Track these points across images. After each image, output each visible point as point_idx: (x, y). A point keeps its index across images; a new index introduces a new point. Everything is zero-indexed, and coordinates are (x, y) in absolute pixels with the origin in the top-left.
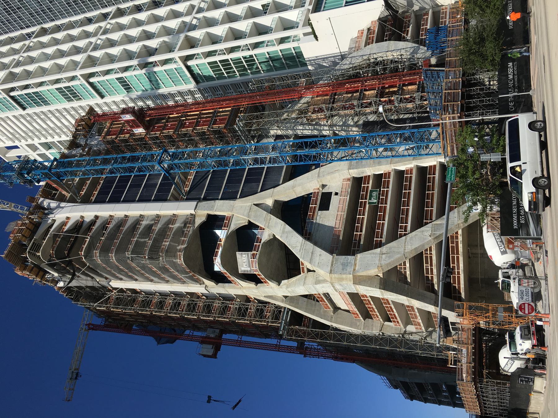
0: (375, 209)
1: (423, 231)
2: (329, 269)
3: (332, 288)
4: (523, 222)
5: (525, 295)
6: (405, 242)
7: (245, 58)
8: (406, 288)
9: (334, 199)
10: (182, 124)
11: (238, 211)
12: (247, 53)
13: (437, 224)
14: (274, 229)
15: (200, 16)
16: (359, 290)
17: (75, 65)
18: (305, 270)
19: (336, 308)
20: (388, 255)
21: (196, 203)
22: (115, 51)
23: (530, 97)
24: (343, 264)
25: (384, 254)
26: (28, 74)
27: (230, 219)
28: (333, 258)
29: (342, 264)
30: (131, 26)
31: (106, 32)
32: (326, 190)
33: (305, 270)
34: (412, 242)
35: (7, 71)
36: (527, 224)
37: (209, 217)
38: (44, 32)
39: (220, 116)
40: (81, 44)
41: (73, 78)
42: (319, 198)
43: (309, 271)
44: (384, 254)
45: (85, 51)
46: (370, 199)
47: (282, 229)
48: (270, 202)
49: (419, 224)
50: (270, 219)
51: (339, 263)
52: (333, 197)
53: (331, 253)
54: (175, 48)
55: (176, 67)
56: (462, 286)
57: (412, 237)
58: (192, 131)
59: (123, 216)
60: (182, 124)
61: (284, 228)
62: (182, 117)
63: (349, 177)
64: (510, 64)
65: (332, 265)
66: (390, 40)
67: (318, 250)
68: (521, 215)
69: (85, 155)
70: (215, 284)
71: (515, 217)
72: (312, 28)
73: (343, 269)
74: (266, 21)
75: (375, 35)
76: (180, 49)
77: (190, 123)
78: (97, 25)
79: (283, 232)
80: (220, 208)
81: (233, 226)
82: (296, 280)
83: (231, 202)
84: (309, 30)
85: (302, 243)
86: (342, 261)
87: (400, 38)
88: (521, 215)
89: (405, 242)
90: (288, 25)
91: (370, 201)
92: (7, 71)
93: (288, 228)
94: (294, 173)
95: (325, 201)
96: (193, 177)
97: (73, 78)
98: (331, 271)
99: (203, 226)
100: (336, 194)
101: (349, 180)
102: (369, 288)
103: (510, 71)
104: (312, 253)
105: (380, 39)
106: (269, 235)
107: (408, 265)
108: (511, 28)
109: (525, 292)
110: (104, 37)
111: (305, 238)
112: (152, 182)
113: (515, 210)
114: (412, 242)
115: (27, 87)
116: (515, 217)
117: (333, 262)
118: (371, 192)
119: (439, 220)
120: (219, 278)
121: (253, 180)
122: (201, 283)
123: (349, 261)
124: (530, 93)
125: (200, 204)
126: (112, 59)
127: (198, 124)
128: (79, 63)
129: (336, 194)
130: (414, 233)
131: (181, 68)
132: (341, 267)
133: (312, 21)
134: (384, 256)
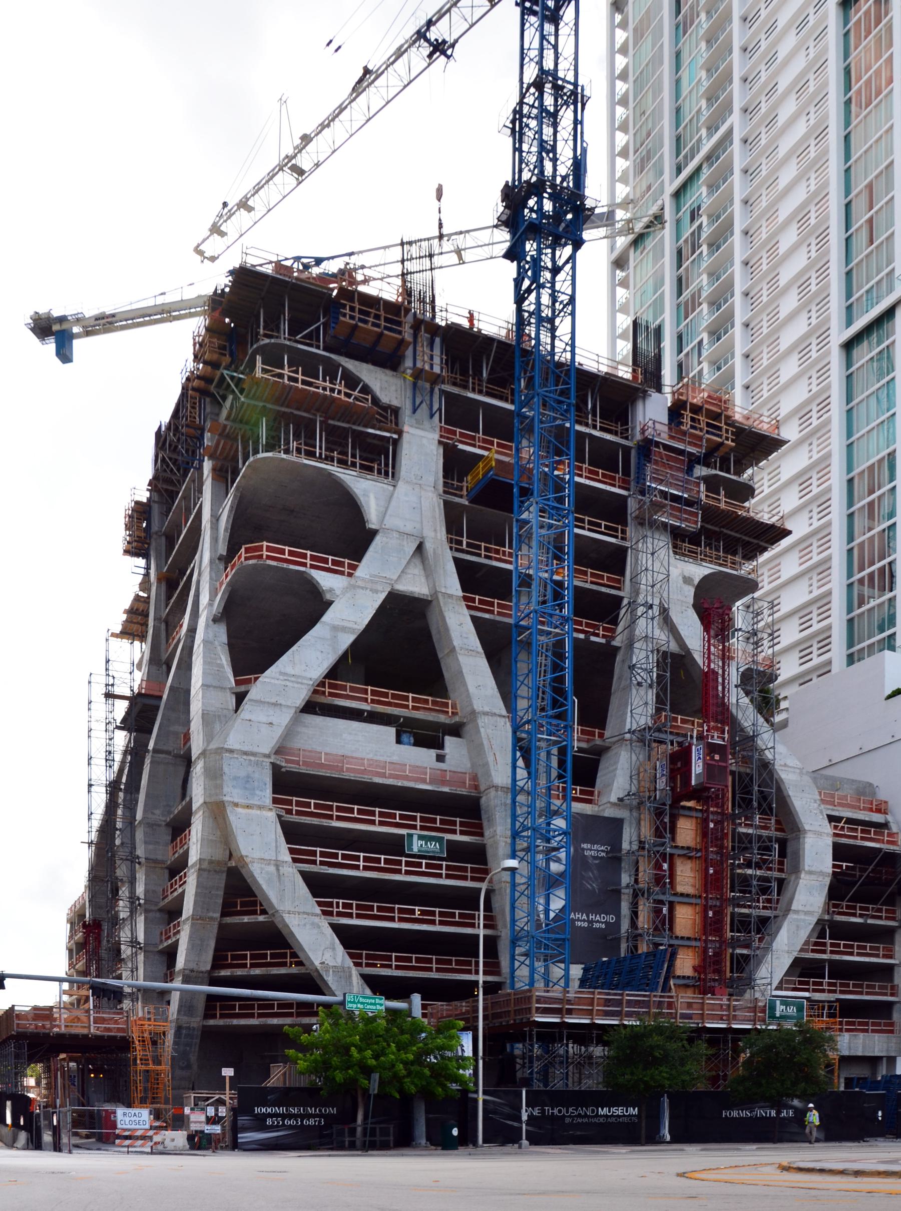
0: (396, 846)
1: (334, 949)
4: (269, 1122)
5: (133, 1119)
6: (308, 914)
8: (211, 914)
13: (350, 976)
14: (351, 604)
16: (197, 816)
18: (242, 688)
20: (275, 879)
24: (248, 779)
25: (278, 870)
28: (265, 756)
29: (248, 777)
33: (242, 688)
34: (308, 926)
36: (264, 1128)
44: (278, 870)
46: (421, 837)
47: (346, 624)
49: (350, 938)
50: (376, 592)
51: (250, 769)
52: (433, 753)
56: (235, 1022)
57: (319, 927)
61: (344, 629)
63: (482, 788)
65: (246, 753)
68: (283, 1121)
71: (282, 1110)
82: (222, 666)
85: (305, 678)
88: (283, 1121)
89: (308, 914)
91: (415, 838)
101: (476, 787)
104: (275, 705)
106: (331, 590)
107: (261, 918)
109: (138, 1119)
114: (308, 926)
117: (254, 754)
118: (440, 840)
119: (361, 981)
123: (258, 792)
124: (525, 1142)
130: (329, 931)
134: (272, 869)
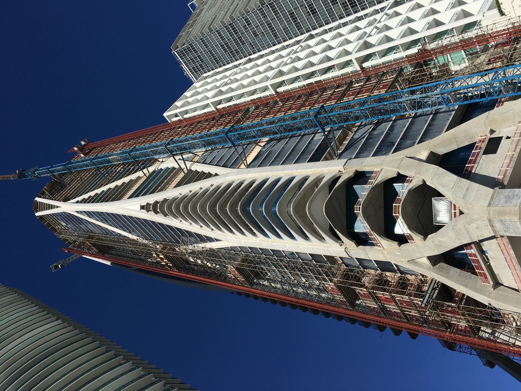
3: (490, 228)
9: (504, 145)
19: (497, 284)
29: (506, 197)
32: (494, 136)
39: (383, 83)
48: (424, 155)
52: (504, 142)
69: (210, 26)
70: (355, 245)
73: (506, 202)
80: (368, 163)
86: (506, 194)
92: (218, 90)
100: (508, 138)
104: (467, 189)
111: (460, 176)
120: (362, 240)
123: (516, 194)
129: (508, 138)
132: (504, 200)
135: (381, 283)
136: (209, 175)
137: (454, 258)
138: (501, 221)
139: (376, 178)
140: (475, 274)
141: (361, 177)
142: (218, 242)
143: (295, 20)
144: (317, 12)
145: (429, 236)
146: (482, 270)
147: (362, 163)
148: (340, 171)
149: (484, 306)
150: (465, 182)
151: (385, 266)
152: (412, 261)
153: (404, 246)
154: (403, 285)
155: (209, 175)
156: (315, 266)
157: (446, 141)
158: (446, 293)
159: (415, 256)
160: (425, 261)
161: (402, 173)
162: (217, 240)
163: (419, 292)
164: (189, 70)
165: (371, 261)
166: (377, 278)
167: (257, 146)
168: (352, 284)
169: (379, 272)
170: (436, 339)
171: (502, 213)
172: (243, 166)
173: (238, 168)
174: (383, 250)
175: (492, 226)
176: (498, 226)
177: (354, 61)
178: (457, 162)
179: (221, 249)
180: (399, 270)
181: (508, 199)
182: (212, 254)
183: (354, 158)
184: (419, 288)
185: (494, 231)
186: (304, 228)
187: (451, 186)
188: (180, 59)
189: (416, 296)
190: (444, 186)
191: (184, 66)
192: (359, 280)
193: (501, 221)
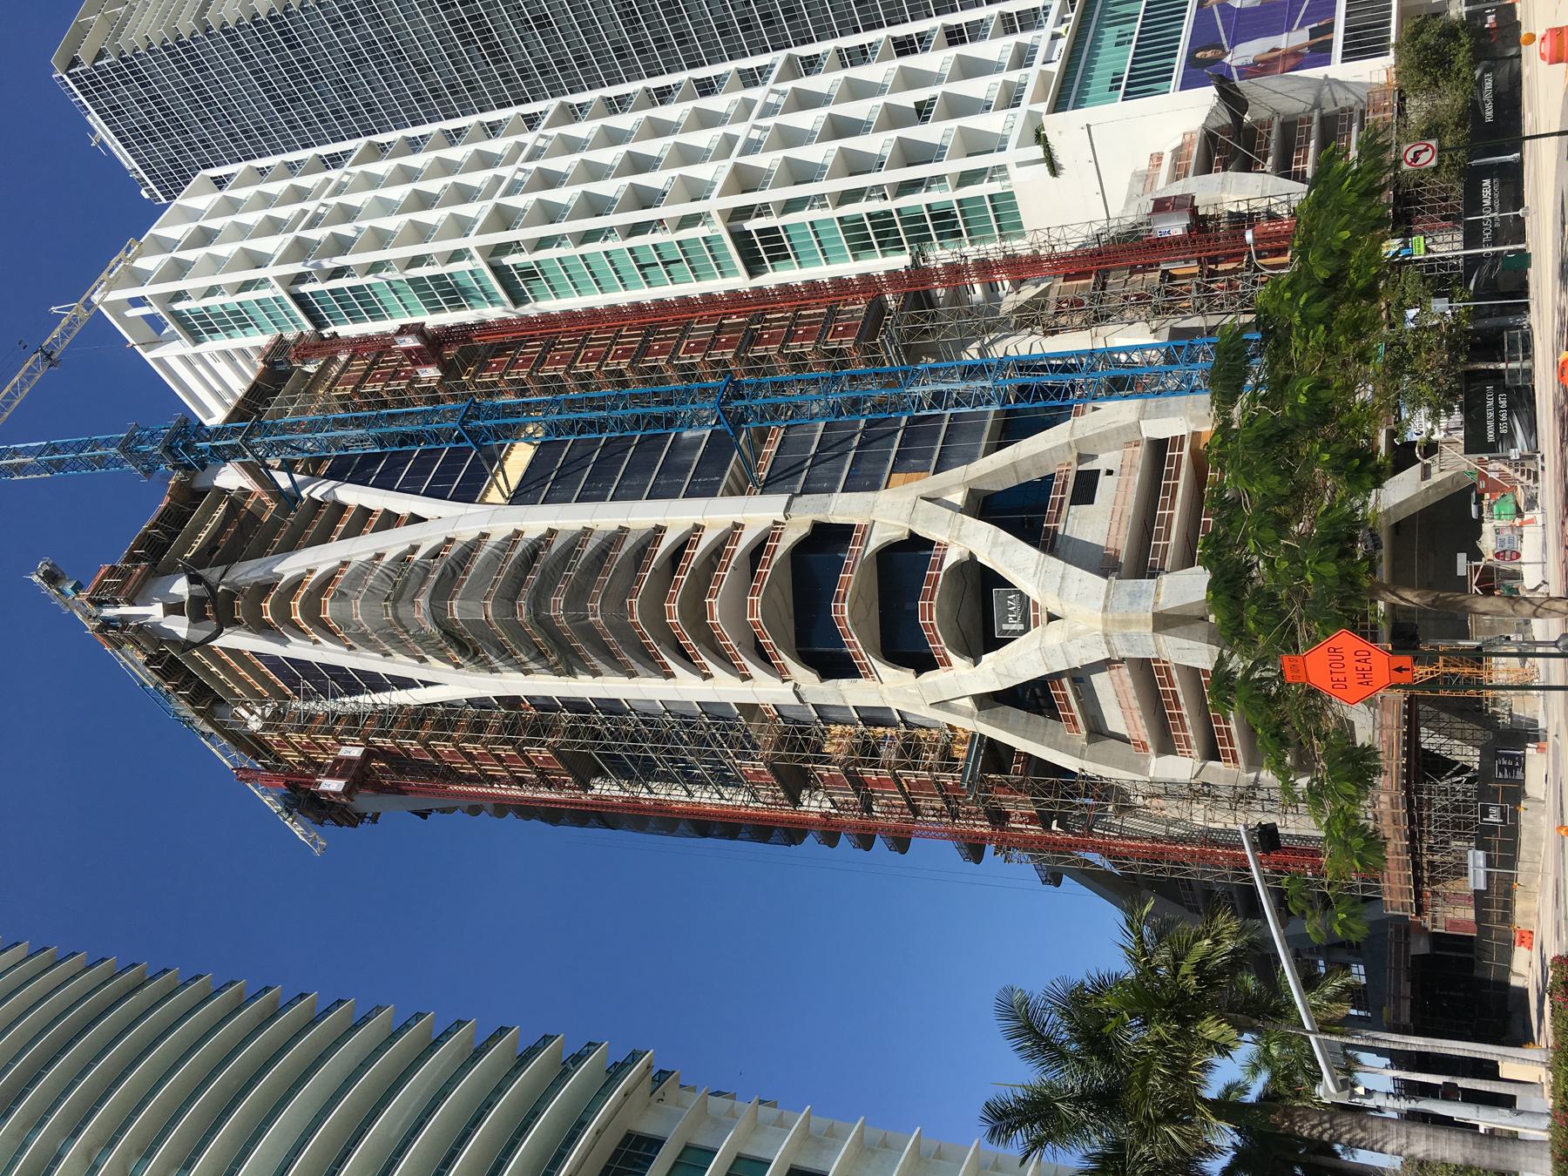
2: (1101, 604)
4: (1503, 431)
7: (870, 216)
9: (1104, 482)
10: (752, 337)
11: (885, 513)
12: (877, 206)
15: (770, 122)
17: (462, 226)
18: (1043, 617)
21: (785, 498)
22: (563, 195)
23: (1520, 221)
26: (341, 245)
27: (867, 530)
30: (392, 181)
31: (536, 154)
35: (290, 237)
37: (818, 527)
38: (379, 152)
40: (284, 212)
41: (457, 256)
42: (1071, 481)
43: (1052, 618)
45: (489, 195)
52: (1102, 478)
53: (1106, 576)
54: (711, 191)
55: (708, 234)
58: (780, 352)
59: (615, 528)
60: (752, 337)
61: (996, 537)
62: (751, 322)
64: (1487, 182)
65: (1107, 597)
66: (1225, 169)
67: (1075, 571)
71: (1490, 425)
72: (1048, 150)
73: (1131, 603)
74: (929, 133)
75: (1193, 161)
76: (722, 194)
77: (771, 335)
78: (512, 140)
79: (995, 544)
80: (841, 508)
81: (875, 543)
83: (869, 495)
84: (1038, 152)
87: (1247, 166)
90: (977, 144)
93: (1004, 536)
94: (1012, 429)
95: (1085, 488)
96: (774, 450)
97: (457, 256)
98: (1105, 607)
99: (801, 548)
100: (1110, 473)
102: (1186, 643)
103: (1486, 193)
104: (1063, 578)
105: (1206, 167)
108: (1488, 120)
110: (333, 201)
112: (679, 460)
113: (1490, 415)
115: (338, 273)
116: (1490, 425)
117: (1108, 590)
121: (922, 444)
122: (781, 673)
124: (1520, 212)
125: (797, 500)
126: (550, 213)
127: (791, 335)
128: (475, 221)
129: (1110, 473)
131: (720, 238)
133: (1049, 132)
135: (868, 751)
136: (390, 520)
137: (1033, 698)
138: (1124, 635)
139: (865, 540)
140: (1056, 717)
141: (829, 539)
142: (429, 688)
143: (485, 34)
144: (550, 24)
145: (985, 657)
146: (1070, 710)
147: (826, 506)
148: (776, 523)
149: (1072, 774)
150: (1056, 564)
151: (874, 717)
152: (942, 705)
153: (929, 677)
154: (911, 750)
155: (390, 520)
156: (708, 726)
157: (998, 466)
158: (996, 756)
159: (944, 694)
160: (968, 703)
161: (922, 532)
162: (427, 684)
163: (948, 759)
164: (116, 134)
165: (847, 708)
166: (856, 741)
167: (520, 445)
168: (807, 760)
169: (861, 727)
170: (951, 844)
171: (1126, 623)
172: (494, 495)
173: (482, 502)
174: (887, 687)
175: (1108, 643)
176: (1117, 642)
177: (716, 217)
178: (1022, 511)
179: (435, 704)
180: (904, 721)
181: (1134, 597)
182: (421, 715)
183: (803, 493)
184: (946, 754)
185: (1110, 651)
186: (698, 645)
187: (1032, 571)
188: (81, 97)
189: (943, 769)
190: (1017, 570)
191: (94, 119)
192: (819, 749)
193: (1124, 635)
